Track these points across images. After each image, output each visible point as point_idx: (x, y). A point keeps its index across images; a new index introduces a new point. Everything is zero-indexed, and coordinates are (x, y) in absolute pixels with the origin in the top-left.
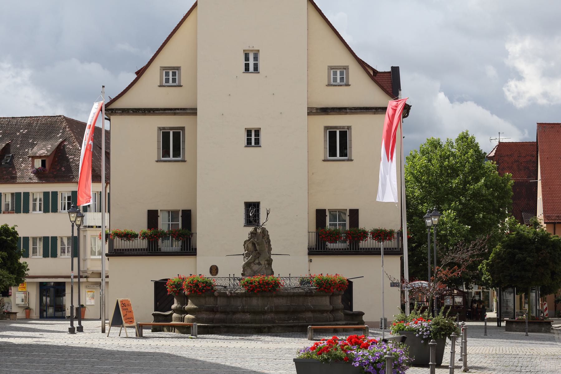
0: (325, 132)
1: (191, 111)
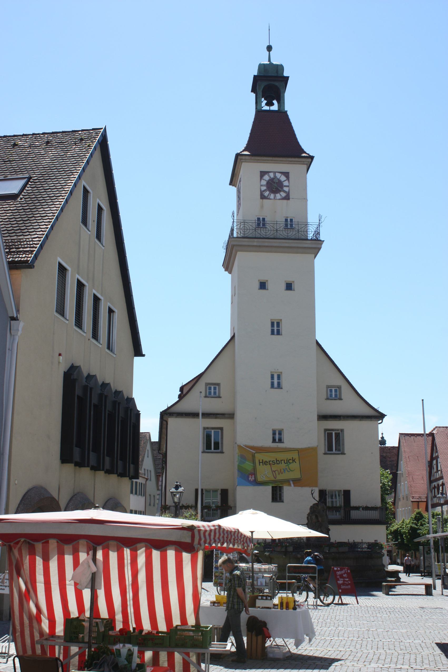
0: (325, 433)
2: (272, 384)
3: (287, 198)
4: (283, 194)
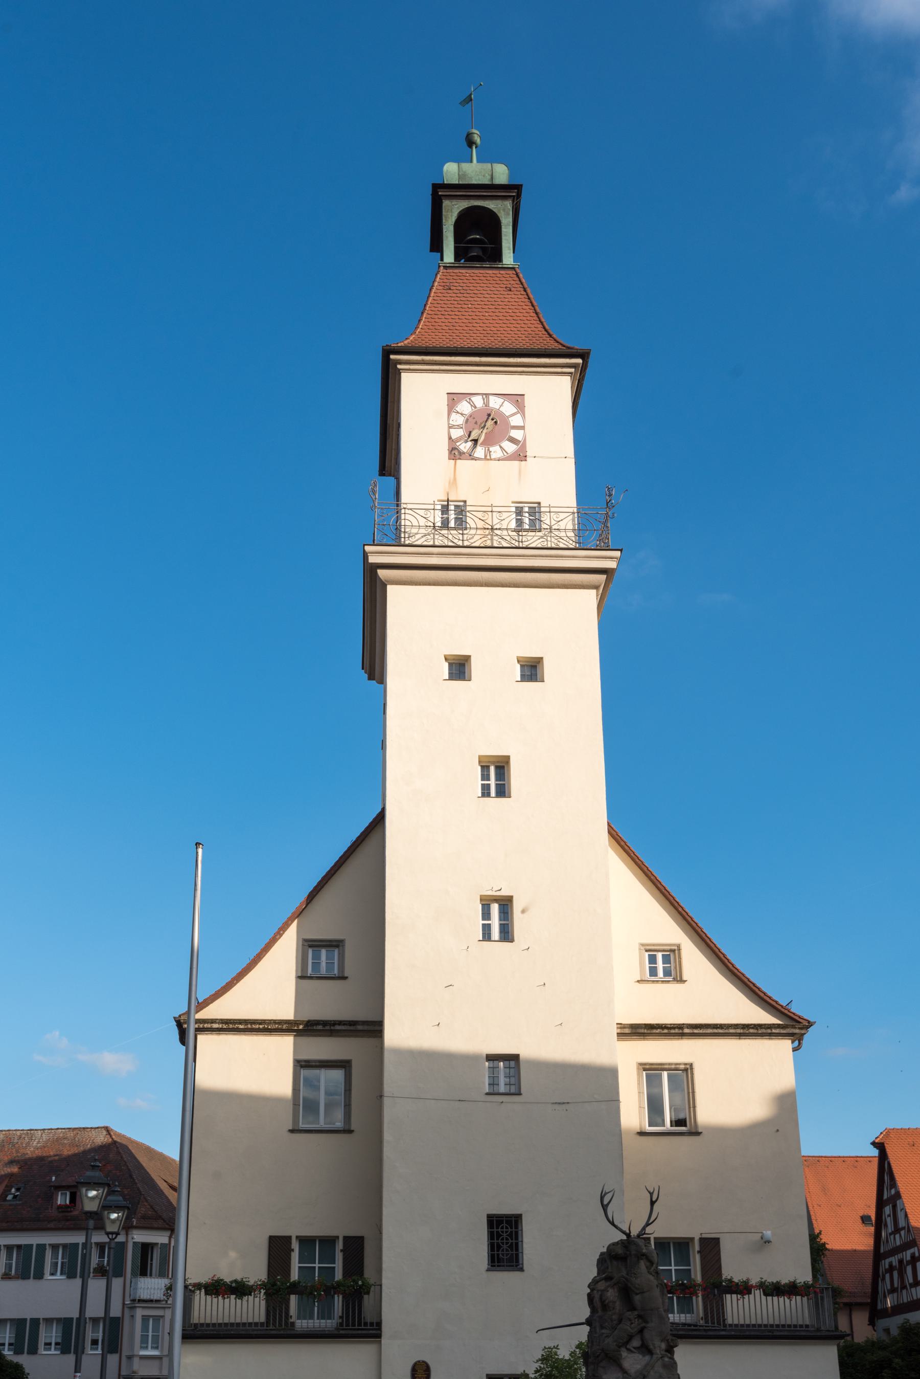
1: (366, 1028)
2: (487, 930)
3: (521, 456)
4: (510, 448)
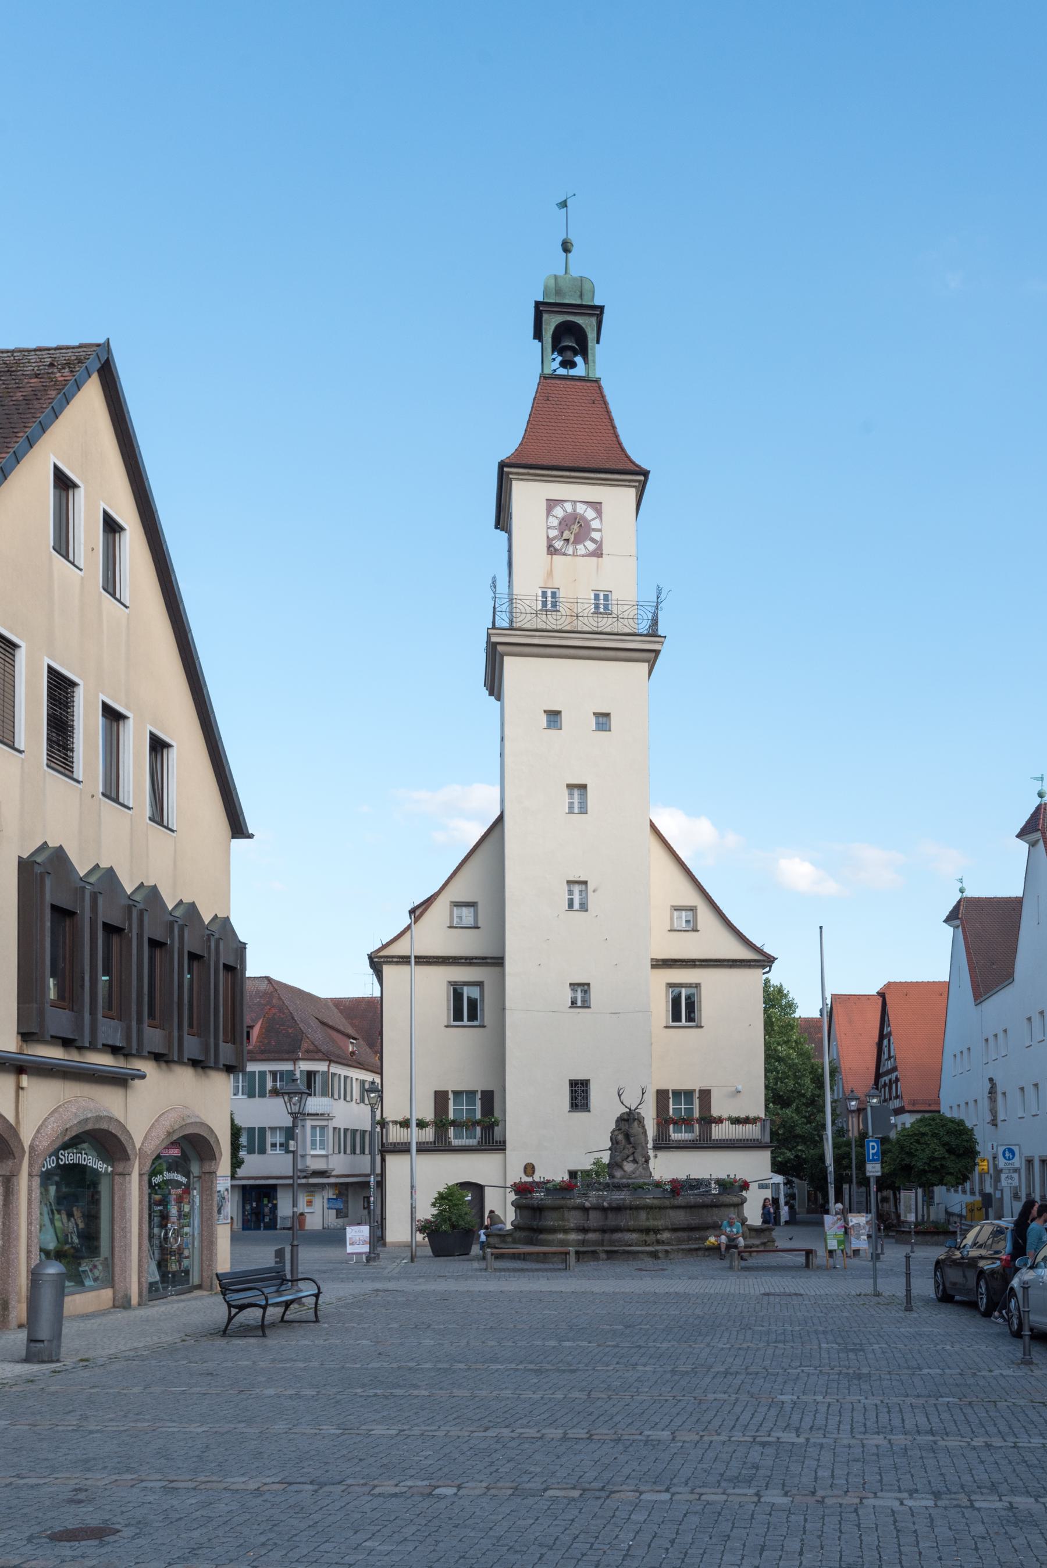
0: (667, 991)
2: (571, 904)
3: (598, 553)
4: (591, 546)
